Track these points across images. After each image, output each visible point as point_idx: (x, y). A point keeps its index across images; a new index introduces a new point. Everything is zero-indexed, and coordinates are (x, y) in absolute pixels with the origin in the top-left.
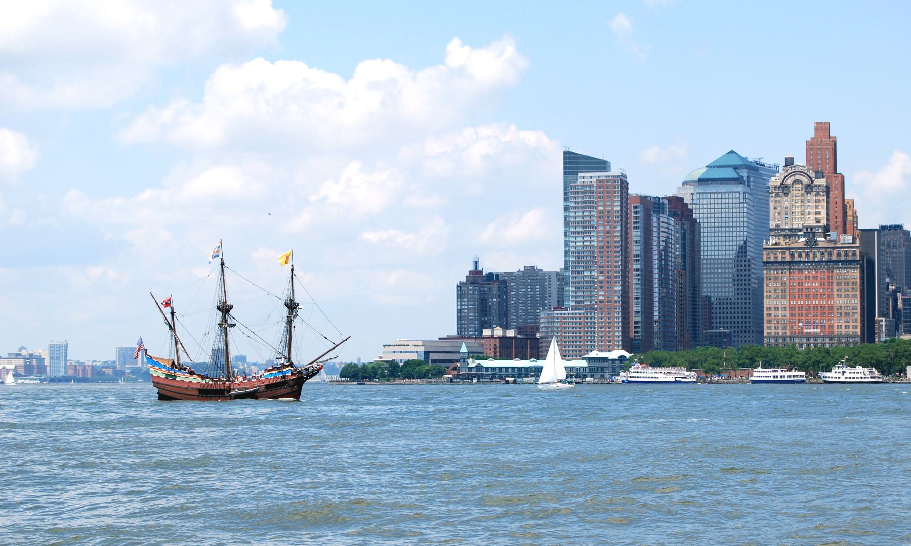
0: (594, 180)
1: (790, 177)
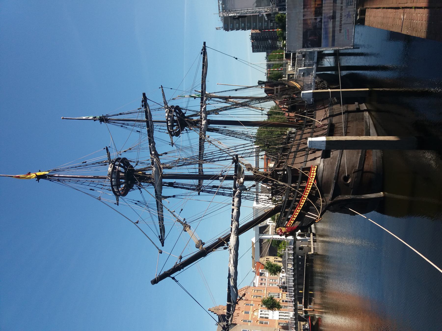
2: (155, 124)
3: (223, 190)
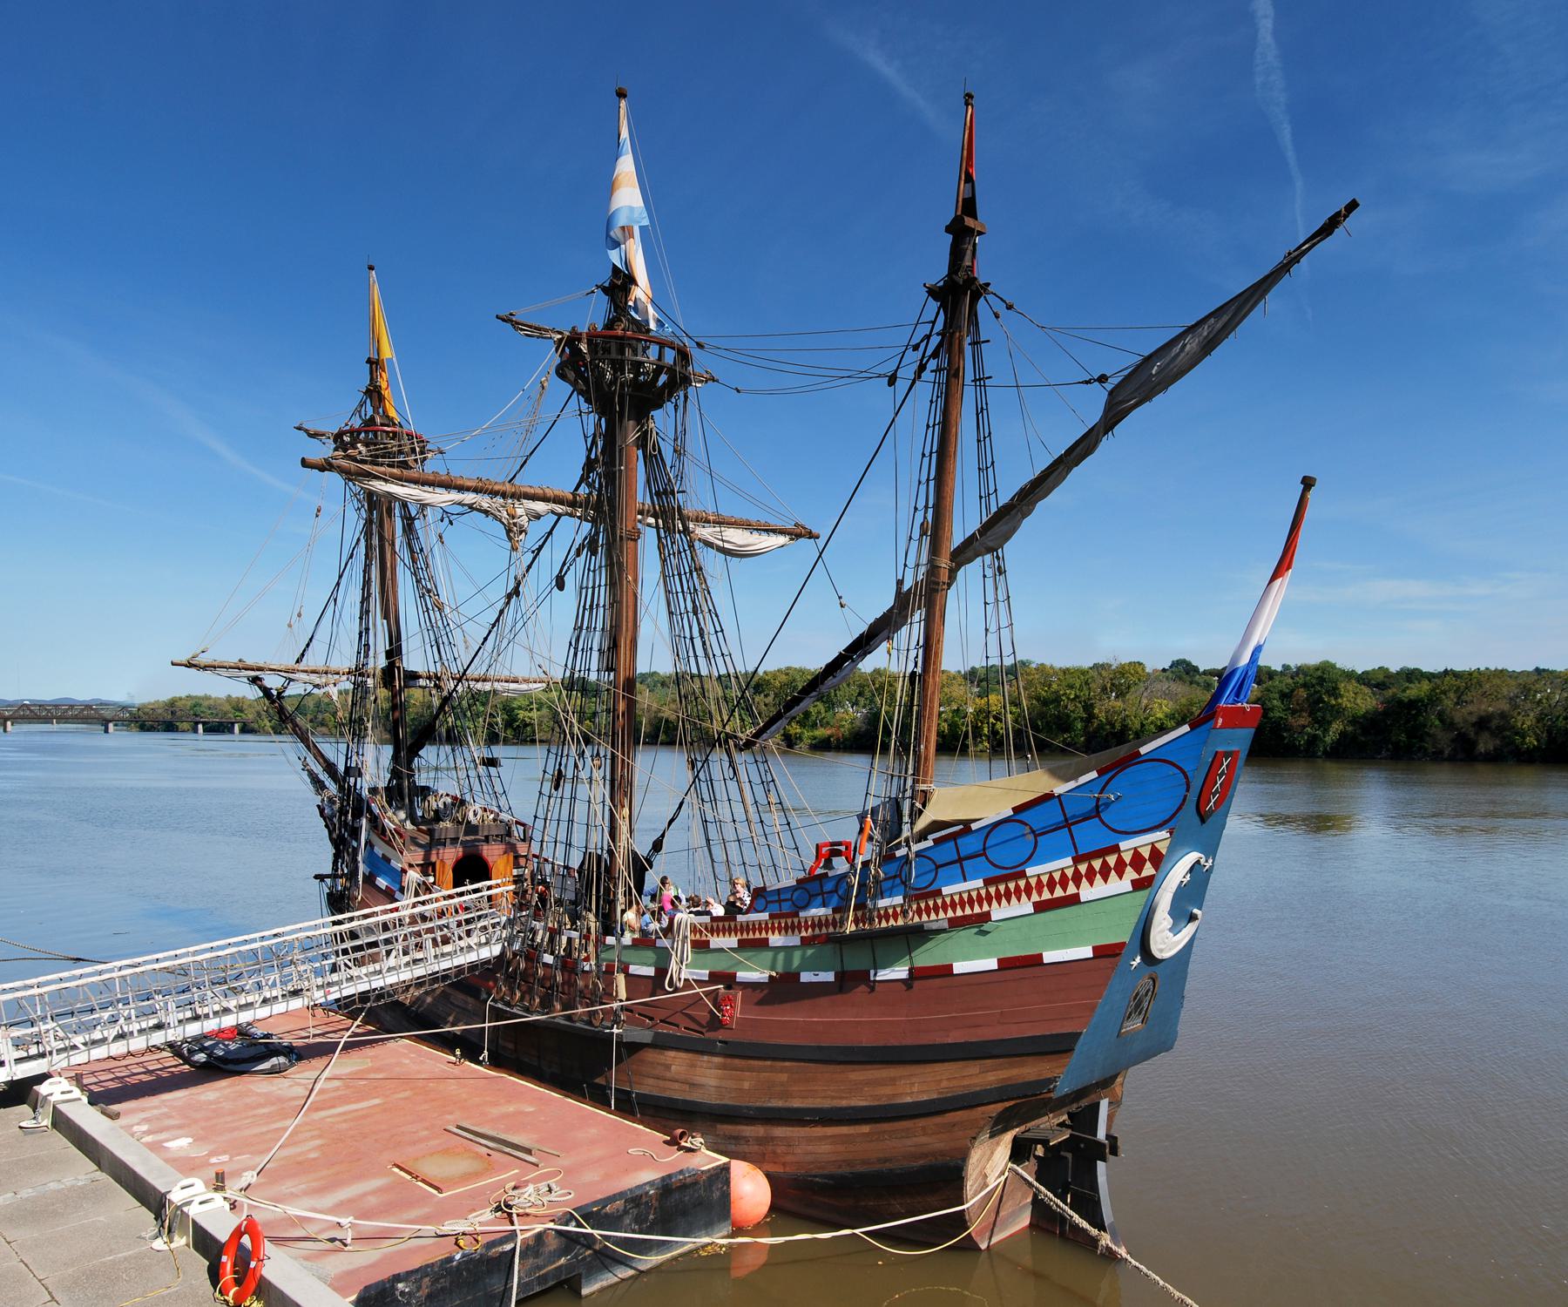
0: (1203, 680)
1: (338, 626)
2: (953, 843)
3: (930, 505)
